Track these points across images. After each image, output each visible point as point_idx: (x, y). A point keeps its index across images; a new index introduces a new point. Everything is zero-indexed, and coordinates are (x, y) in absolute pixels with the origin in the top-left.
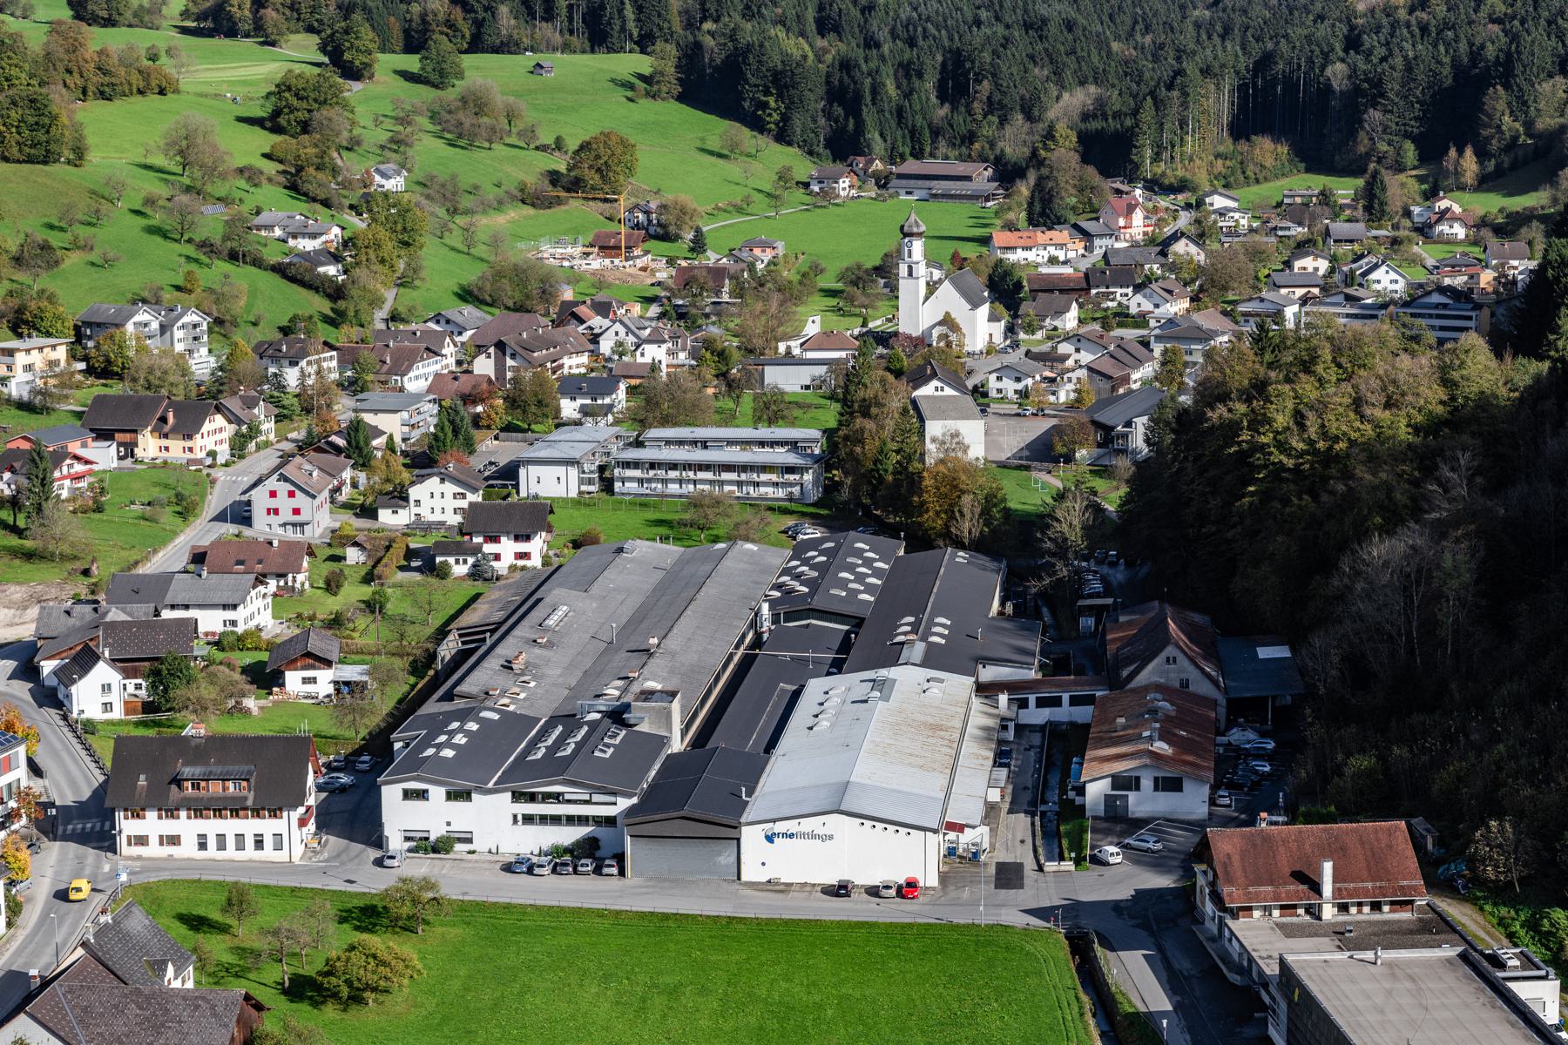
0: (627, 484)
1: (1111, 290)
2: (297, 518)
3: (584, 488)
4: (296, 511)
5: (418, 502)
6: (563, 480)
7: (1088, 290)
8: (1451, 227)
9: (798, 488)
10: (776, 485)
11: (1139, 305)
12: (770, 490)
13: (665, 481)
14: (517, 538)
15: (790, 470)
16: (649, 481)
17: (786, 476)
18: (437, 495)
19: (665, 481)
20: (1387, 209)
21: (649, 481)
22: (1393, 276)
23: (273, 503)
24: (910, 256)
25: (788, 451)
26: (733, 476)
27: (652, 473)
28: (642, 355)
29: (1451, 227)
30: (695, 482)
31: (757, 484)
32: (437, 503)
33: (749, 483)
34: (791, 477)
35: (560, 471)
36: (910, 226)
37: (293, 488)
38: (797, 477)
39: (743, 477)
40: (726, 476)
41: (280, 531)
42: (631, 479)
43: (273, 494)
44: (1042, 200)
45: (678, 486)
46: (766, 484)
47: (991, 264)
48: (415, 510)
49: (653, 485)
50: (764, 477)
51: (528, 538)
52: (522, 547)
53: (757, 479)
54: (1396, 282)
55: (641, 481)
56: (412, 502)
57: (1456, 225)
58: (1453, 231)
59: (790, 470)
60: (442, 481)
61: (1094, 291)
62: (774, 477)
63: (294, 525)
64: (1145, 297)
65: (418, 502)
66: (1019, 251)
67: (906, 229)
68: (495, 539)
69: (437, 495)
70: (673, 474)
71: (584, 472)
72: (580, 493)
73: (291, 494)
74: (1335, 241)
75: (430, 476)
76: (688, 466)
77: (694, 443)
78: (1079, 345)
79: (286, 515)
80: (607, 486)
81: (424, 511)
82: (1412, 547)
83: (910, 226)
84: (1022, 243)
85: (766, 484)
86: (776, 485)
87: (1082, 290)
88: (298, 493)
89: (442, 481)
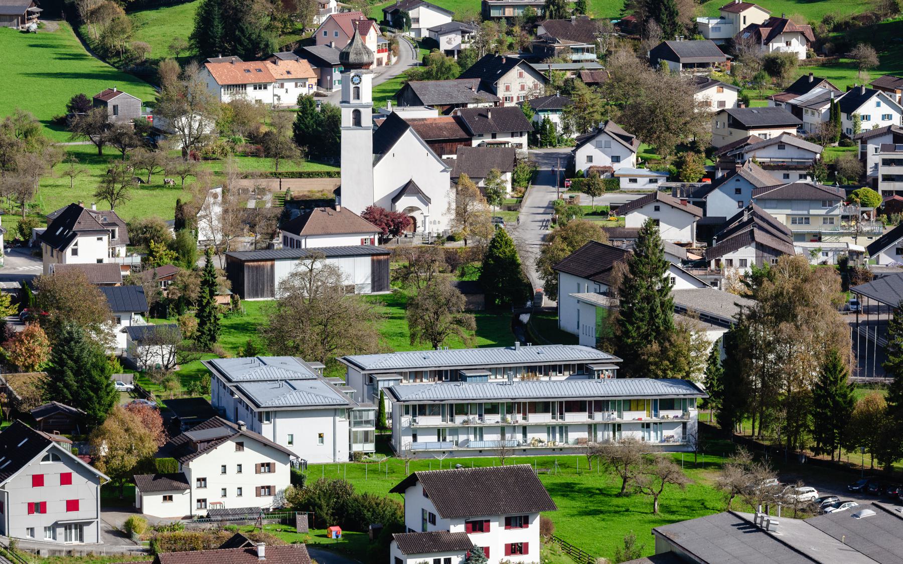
0: (420, 439)
1: (499, 139)
2: (73, 516)
3: (357, 448)
4: (73, 505)
5: (202, 481)
6: (328, 438)
7: (468, 142)
8: (788, 44)
9: (679, 430)
10: (646, 426)
11: (590, 159)
12: (638, 435)
13: (480, 432)
14: (510, 523)
15: (668, 404)
16: (455, 431)
17: (662, 413)
18: (232, 469)
19: (480, 432)
20: (678, 20)
21: (455, 431)
22: (886, 109)
23: (37, 495)
24: (358, 96)
25: (570, 378)
26: (581, 417)
27: (459, 419)
28: (75, 252)
29: (788, 44)
30: (524, 430)
31: (617, 427)
32: (232, 480)
33: (465, 429)
34: (670, 414)
35: (324, 423)
36: (358, 53)
37: (67, 470)
38: (679, 413)
39: (598, 417)
40: (571, 418)
41: (47, 538)
42: (427, 430)
43: (38, 481)
44: (224, 18)
45: (434, 438)
46: (631, 426)
47: (377, 103)
48: (198, 493)
49: (462, 438)
50: (629, 416)
51: (523, 522)
52: (517, 535)
53: (618, 420)
54: (889, 117)
55: (440, 433)
56: (194, 483)
57: (794, 41)
58: (790, 50)
59: (668, 404)
60: (240, 446)
61: (475, 143)
62: (643, 416)
63: (68, 526)
64: (598, 146)
65: (202, 481)
66: (250, 89)
67: (352, 58)
68: (480, 527)
69: (232, 469)
70: (492, 419)
71: (358, 423)
72: (353, 457)
73: (66, 479)
74: (685, 66)
75: (221, 440)
76: (512, 407)
77: (440, 375)
78: (656, 215)
79: (57, 512)
80: (385, 445)
81: (212, 494)
82: (181, 480)
83: (358, 53)
84: (252, 78)
85: (631, 426)
86: (646, 426)
87: (460, 141)
88: (76, 477)
89: (240, 446)
